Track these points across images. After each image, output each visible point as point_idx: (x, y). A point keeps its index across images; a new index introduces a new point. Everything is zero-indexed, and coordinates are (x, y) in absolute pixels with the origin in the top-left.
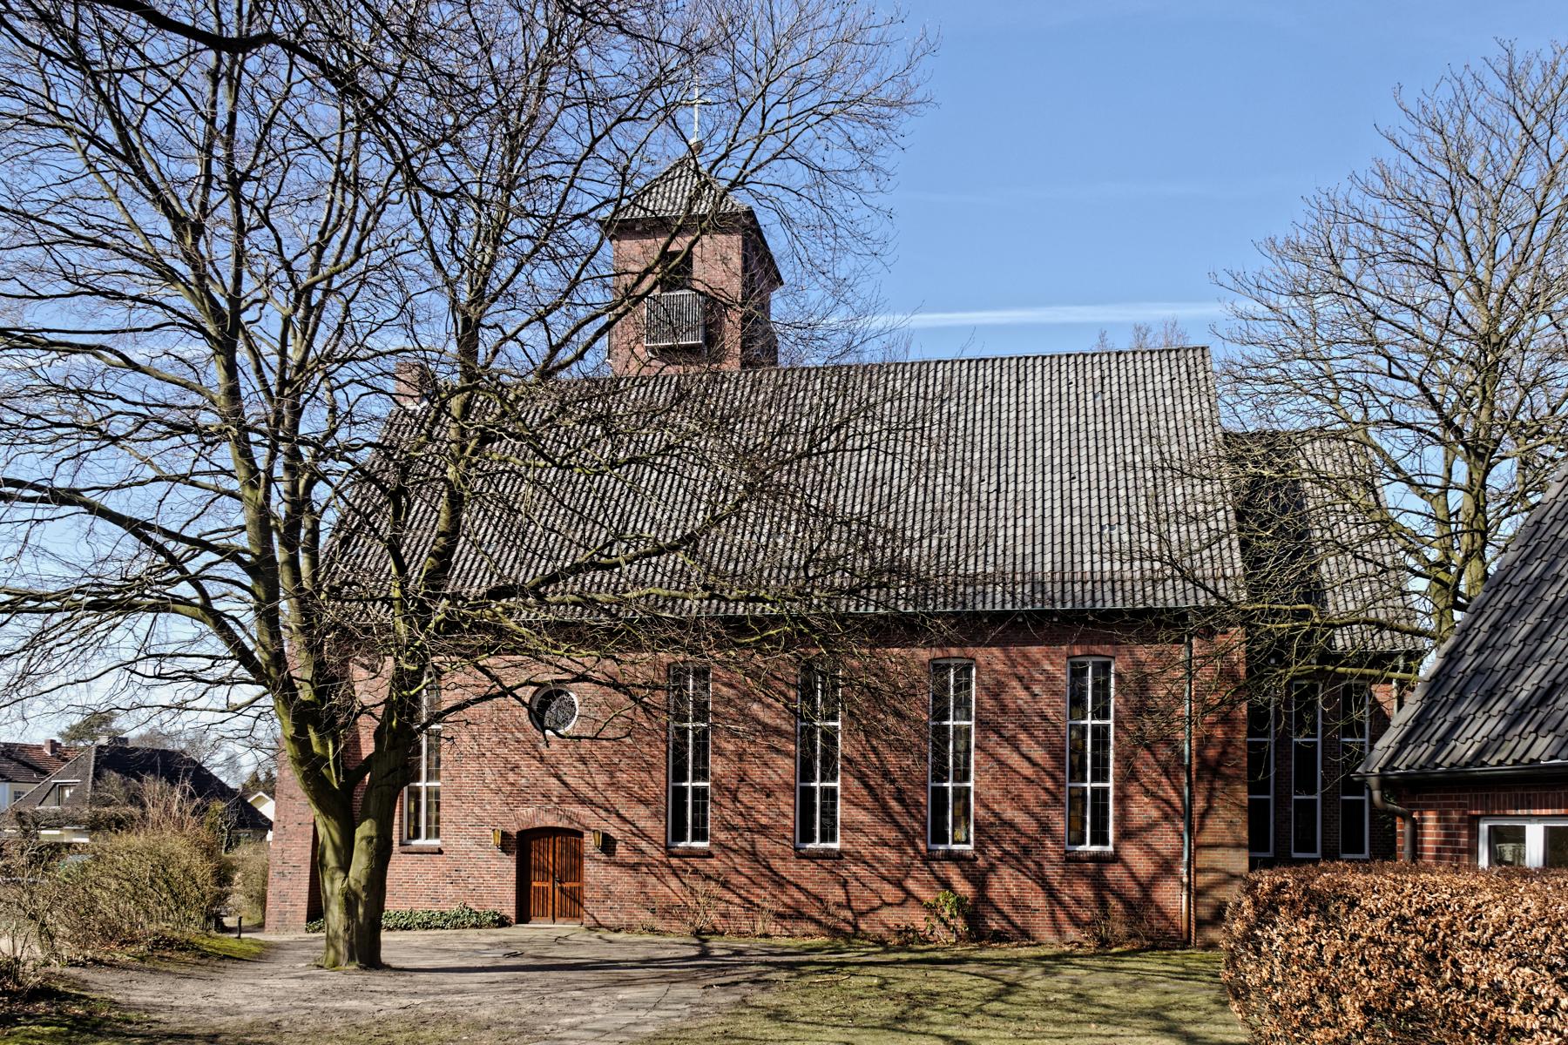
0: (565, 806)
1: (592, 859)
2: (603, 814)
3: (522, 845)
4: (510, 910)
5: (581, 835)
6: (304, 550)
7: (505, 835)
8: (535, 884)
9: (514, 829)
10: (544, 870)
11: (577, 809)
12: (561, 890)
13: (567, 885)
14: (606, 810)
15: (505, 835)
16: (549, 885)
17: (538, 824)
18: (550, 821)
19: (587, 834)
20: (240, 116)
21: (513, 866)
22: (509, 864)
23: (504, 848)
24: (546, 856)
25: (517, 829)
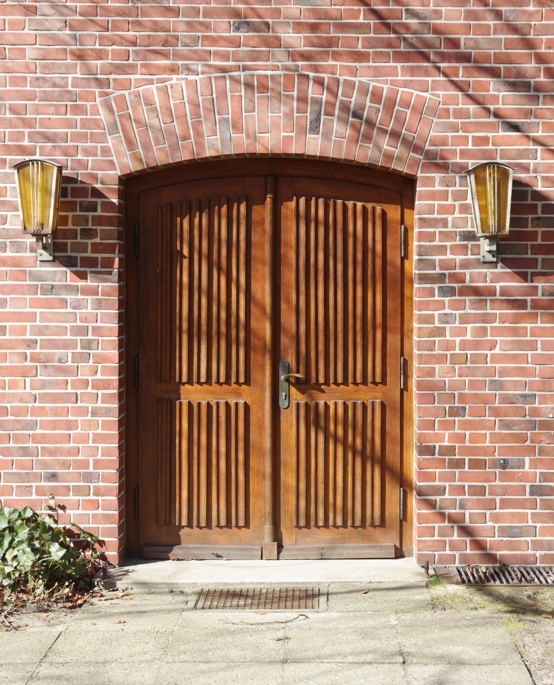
0: (337, 68)
1: (453, 285)
2: (504, 99)
3: (142, 232)
4: (96, 513)
5: (399, 188)
6: (185, 257)
7: (71, 192)
8: (191, 394)
9: (107, 163)
10: (232, 334)
11: (395, 79)
12: (314, 418)
13: (332, 399)
14: (519, 84)
15: (71, 192)
16: (258, 397)
17: (216, 143)
18: (271, 129)
19: (430, 187)
20: (349, 661)
21: (108, 320)
22: (88, 313)
23: (61, 246)
24: (224, 268)
25: (127, 163)
